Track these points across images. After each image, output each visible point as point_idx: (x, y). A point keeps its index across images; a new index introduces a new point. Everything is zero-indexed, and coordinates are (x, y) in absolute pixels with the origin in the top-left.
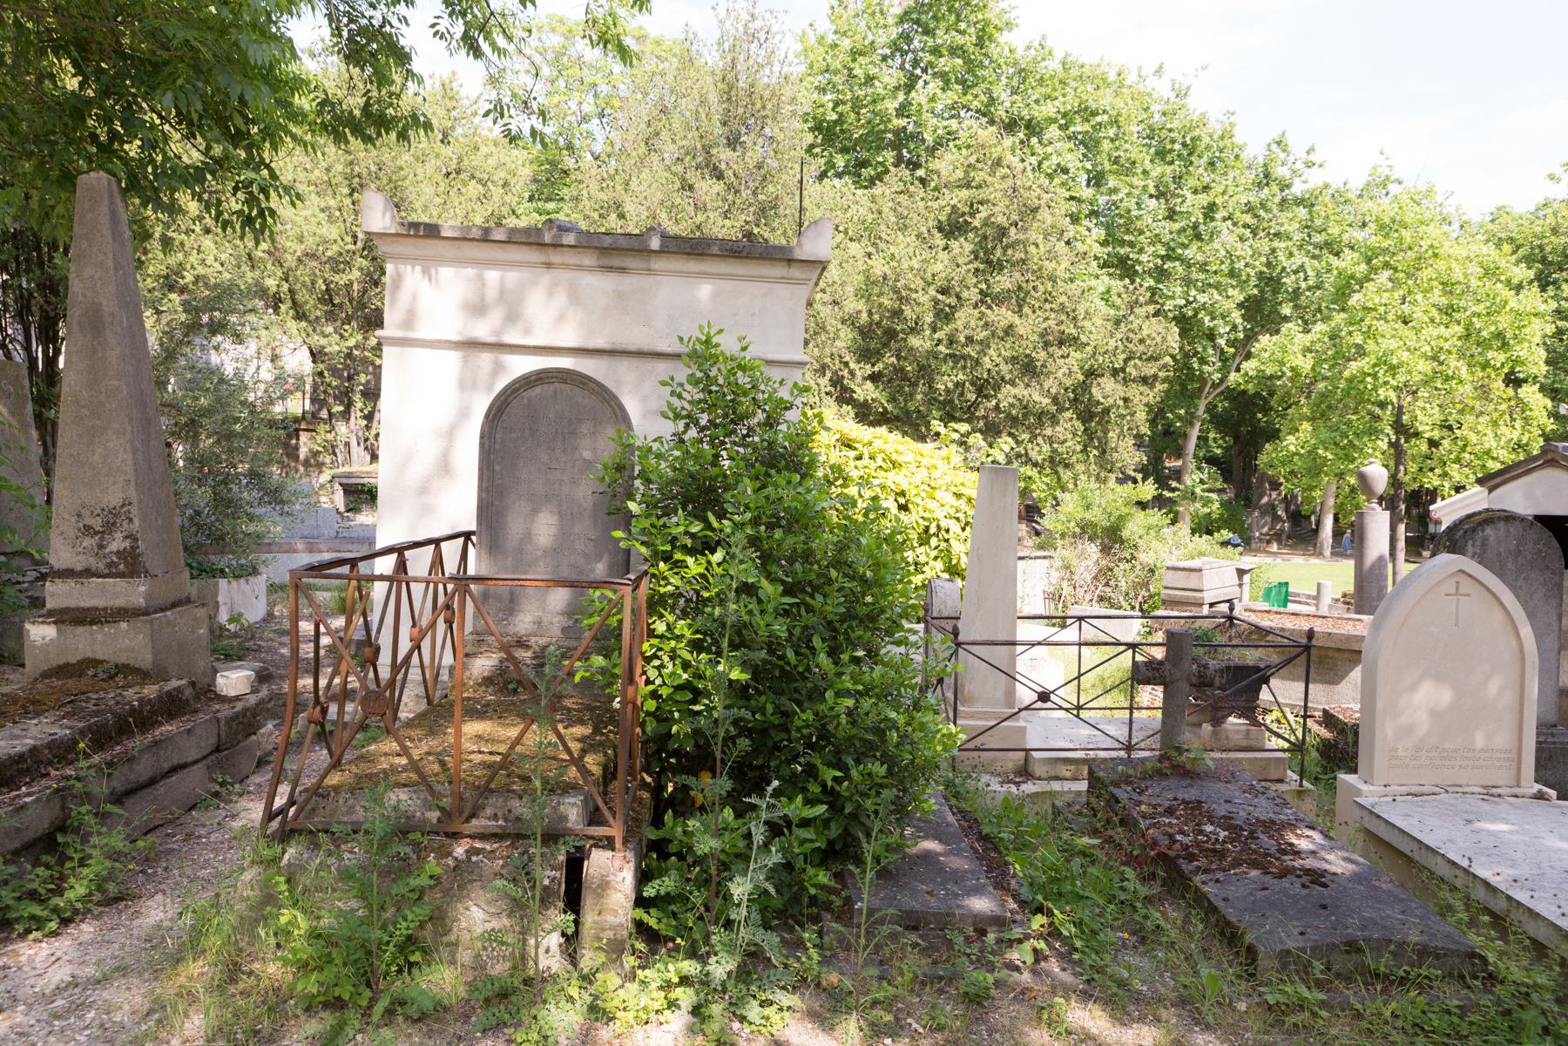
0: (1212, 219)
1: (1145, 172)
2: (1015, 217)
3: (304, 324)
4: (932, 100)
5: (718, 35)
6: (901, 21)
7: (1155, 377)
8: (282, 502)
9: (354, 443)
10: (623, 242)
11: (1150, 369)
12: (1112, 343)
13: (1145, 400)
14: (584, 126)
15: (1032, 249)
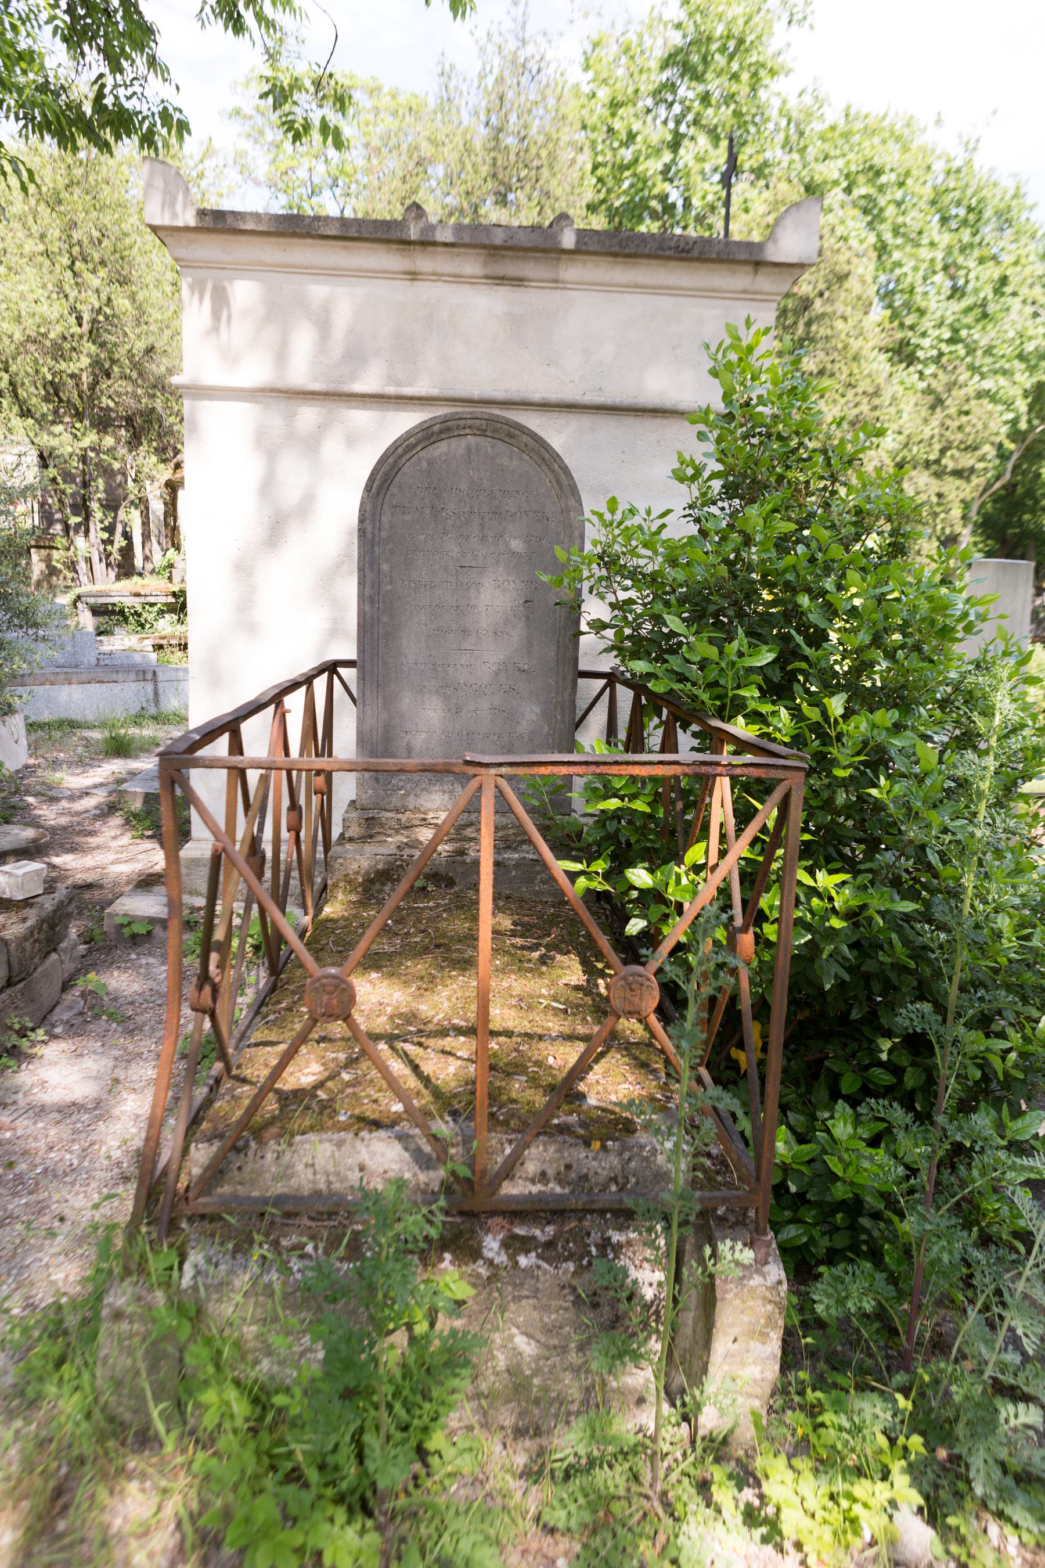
0: (1003, 294)
1: (932, 244)
2: (822, 286)
3: (30, 421)
4: (701, 159)
5: (478, 66)
6: (665, 65)
7: (972, 470)
8: (36, 625)
9: (95, 559)
10: (523, 239)
11: (967, 461)
12: (927, 432)
13: (962, 496)
14: (314, 199)
15: (839, 324)
